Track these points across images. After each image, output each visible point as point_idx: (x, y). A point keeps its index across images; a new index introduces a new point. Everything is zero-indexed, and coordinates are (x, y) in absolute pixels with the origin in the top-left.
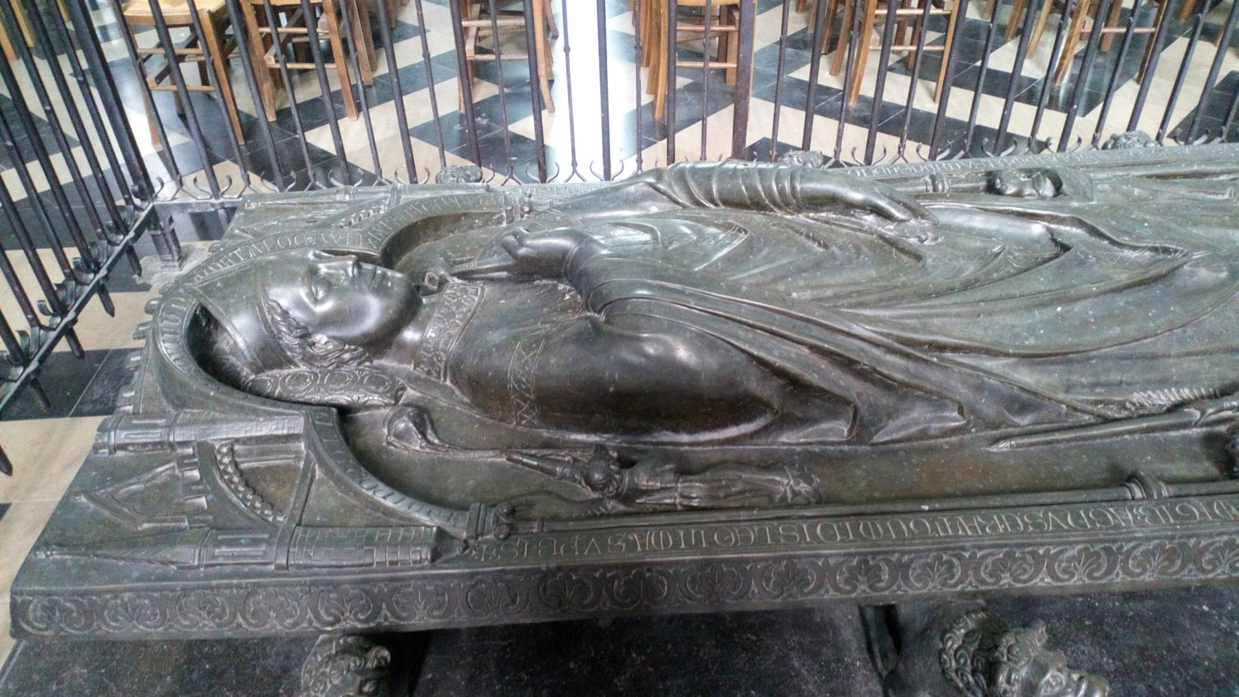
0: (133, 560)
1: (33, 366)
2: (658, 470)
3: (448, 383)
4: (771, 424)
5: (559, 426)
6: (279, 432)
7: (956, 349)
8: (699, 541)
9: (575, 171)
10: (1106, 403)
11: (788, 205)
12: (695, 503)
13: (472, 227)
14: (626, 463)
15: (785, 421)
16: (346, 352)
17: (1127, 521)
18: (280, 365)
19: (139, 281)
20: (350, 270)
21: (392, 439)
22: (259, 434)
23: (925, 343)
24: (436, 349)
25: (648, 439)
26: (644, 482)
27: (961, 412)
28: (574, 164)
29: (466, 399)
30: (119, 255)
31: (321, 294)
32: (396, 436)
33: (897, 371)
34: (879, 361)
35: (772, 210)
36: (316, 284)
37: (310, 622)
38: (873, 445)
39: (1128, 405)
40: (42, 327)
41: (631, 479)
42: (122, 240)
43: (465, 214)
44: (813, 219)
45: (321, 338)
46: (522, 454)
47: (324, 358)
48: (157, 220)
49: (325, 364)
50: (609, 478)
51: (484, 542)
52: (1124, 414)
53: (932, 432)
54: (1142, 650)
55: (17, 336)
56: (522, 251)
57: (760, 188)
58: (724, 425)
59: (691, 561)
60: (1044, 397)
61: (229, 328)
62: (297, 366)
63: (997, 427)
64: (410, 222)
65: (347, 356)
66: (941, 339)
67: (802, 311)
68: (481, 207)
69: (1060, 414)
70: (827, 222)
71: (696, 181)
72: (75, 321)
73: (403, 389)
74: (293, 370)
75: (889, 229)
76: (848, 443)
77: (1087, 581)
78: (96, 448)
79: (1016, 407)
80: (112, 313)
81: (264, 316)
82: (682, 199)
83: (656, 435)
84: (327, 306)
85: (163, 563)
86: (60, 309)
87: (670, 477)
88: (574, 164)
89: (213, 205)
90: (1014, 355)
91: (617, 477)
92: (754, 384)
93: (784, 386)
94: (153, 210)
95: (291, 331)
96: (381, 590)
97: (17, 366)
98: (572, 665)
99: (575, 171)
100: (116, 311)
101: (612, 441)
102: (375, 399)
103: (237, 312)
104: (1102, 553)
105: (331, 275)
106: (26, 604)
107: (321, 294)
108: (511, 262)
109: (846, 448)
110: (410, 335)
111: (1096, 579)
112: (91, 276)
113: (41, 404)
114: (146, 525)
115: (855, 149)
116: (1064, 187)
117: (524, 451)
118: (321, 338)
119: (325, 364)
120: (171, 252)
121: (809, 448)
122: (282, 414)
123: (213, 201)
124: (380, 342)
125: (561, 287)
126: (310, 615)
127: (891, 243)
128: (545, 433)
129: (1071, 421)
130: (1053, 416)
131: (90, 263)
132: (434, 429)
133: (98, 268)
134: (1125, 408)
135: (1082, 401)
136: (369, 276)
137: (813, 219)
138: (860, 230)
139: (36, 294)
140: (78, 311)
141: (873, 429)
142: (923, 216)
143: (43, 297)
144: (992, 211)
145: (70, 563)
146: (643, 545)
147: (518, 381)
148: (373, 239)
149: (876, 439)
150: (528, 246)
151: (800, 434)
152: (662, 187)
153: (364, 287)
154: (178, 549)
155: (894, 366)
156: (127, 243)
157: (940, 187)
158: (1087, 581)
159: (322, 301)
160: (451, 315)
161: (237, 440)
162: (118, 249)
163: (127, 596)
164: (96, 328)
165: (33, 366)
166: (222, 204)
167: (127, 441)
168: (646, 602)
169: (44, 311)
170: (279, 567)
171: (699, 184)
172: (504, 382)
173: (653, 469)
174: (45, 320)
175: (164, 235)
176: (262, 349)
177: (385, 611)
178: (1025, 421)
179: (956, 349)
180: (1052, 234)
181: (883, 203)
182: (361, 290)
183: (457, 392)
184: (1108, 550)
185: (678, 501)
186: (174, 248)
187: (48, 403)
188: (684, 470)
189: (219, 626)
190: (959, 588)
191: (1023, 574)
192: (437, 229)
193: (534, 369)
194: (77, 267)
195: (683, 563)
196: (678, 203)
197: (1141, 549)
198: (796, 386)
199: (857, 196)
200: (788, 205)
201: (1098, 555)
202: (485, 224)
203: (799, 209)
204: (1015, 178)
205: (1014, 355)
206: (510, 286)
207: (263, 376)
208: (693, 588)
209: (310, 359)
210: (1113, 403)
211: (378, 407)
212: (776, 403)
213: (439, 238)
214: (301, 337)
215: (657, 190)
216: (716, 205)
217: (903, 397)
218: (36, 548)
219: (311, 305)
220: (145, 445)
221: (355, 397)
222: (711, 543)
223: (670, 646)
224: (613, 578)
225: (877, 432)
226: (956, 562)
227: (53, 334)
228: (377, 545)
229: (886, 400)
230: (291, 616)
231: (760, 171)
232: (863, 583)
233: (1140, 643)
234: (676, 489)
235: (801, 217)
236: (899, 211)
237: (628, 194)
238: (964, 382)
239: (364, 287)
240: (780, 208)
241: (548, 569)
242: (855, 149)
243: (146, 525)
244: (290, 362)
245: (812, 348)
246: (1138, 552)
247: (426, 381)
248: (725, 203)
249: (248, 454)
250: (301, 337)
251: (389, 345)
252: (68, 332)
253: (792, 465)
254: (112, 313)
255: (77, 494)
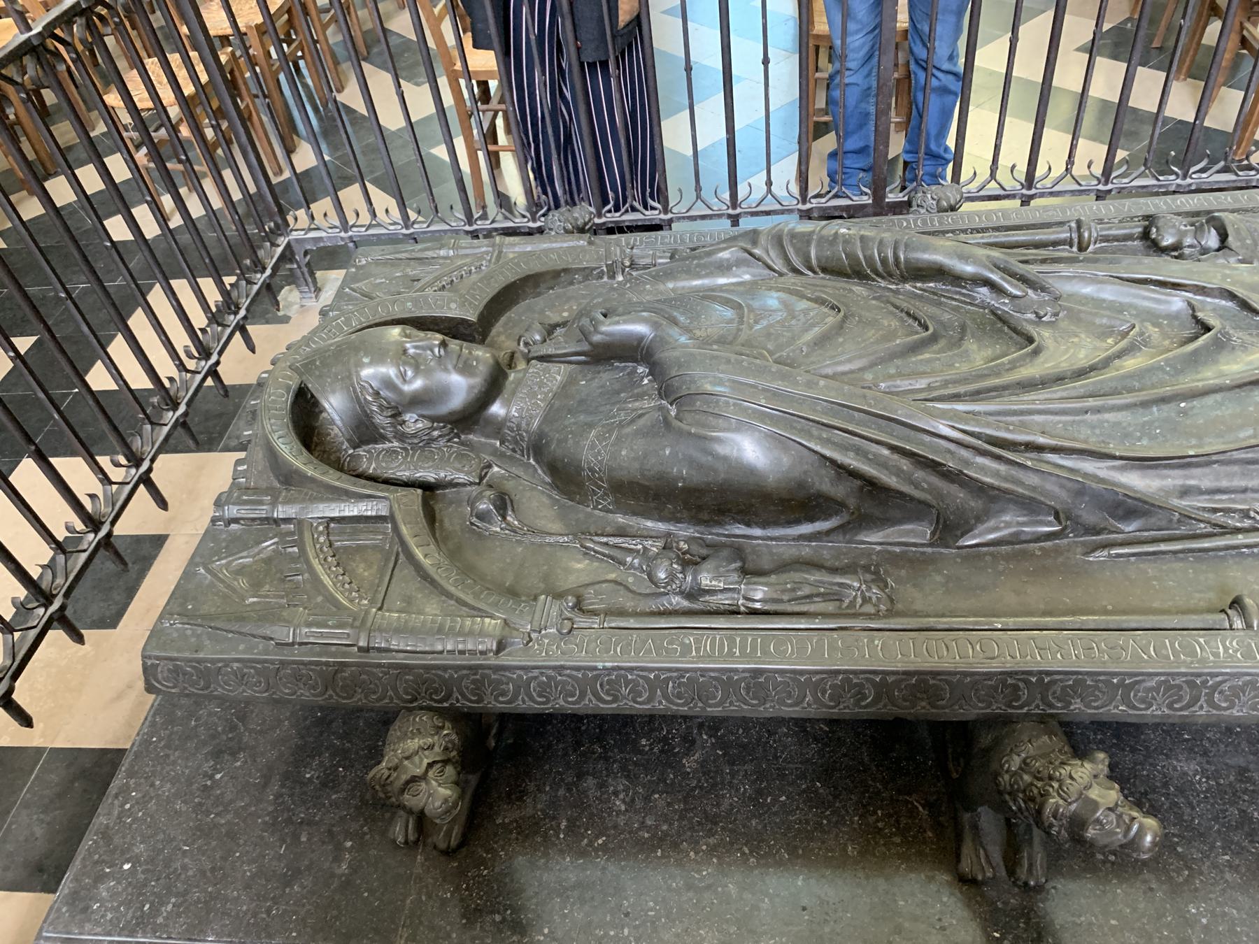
0: (240, 633)
1: (182, 409)
2: (722, 569)
3: (531, 460)
4: (849, 523)
5: (635, 514)
6: (369, 513)
7: (1055, 450)
8: (754, 649)
9: (769, 191)
10: (1227, 511)
11: (891, 275)
12: (758, 606)
13: (572, 283)
14: (689, 562)
15: (862, 521)
16: (435, 429)
17: (1216, 655)
18: (376, 442)
19: (281, 313)
20: (436, 350)
21: (474, 520)
22: (351, 514)
23: (1021, 444)
24: (519, 426)
25: (721, 531)
26: (706, 580)
27: (1057, 517)
28: (698, 188)
29: (548, 479)
30: (258, 293)
31: (410, 373)
32: (477, 517)
33: (986, 475)
34: (967, 463)
35: (874, 280)
36: (405, 363)
37: (391, 699)
38: (959, 548)
39: (1252, 514)
40: (188, 371)
41: (695, 579)
42: (260, 278)
43: (565, 270)
44: (921, 289)
45: (410, 417)
46: (594, 542)
47: (414, 436)
48: (293, 254)
49: (416, 441)
50: (672, 577)
51: (546, 636)
52: (1247, 523)
53: (1023, 537)
54: (1242, 772)
55: (199, 333)
56: (597, 338)
57: (861, 257)
58: (798, 522)
59: (745, 670)
60: (1153, 505)
61: (326, 406)
62: (390, 442)
63: (1098, 533)
64: (508, 282)
65: (436, 433)
66: (1041, 440)
67: (884, 409)
68: (581, 261)
69: (1171, 521)
70: (935, 294)
71: (793, 245)
72: (218, 363)
73: (490, 466)
74: (388, 445)
75: (1004, 305)
76: (931, 545)
77: (1167, 711)
78: (214, 521)
79: (1120, 512)
80: (253, 350)
81: (357, 397)
82: (779, 265)
83: (728, 527)
84: (418, 384)
85: (264, 638)
86: (205, 353)
87: (735, 577)
88: (698, 188)
89: (342, 239)
90: (1121, 458)
91: (680, 576)
92: (825, 483)
93: (861, 488)
94: (289, 245)
95: (382, 411)
96: (451, 676)
97: (168, 410)
98: (644, 742)
99: (769, 191)
100: (257, 350)
101: (684, 532)
102: (462, 477)
103: (334, 392)
104: (1185, 686)
105: (419, 355)
106: (155, 666)
107: (410, 373)
108: (585, 347)
109: (929, 550)
110: (497, 409)
111: (1177, 710)
112: (259, 276)
113: (191, 443)
114: (252, 600)
115: (1014, 166)
116: (1230, 239)
117: (596, 538)
118: (410, 417)
119: (416, 441)
120: (307, 285)
121: (889, 548)
122: (369, 496)
123: (342, 234)
124: (469, 418)
125: (640, 369)
126: (390, 693)
127: (1001, 319)
128: (620, 519)
129: (1183, 530)
130: (1164, 523)
131: (230, 304)
132: (513, 510)
133: (264, 269)
134: (1250, 518)
135: (1198, 509)
136: (455, 357)
137: (921, 289)
138: (971, 304)
139: (181, 340)
140: (220, 353)
141: (959, 533)
142: (1043, 289)
143: (189, 343)
144: (1128, 280)
145: (189, 632)
146: (698, 650)
147: (592, 470)
148: (470, 303)
149: (960, 543)
150: (602, 333)
151: (881, 534)
152: (756, 251)
153: (450, 367)
154: (276, 628)
155: (985, 469)
156: (238, 323)
157: (1086, 235)
158: (1167, 711)
159: (410, 382)
160: (534, 395)
161: (332, 519)
162: (256, 288)
163: (235, 665)
164: (237, 366)
165: (182, 409)
166: (351, 237)
167: (239, 516)
168: (700, 704)
169: (190, 356)
170: (361, 649)
171: (797, 251)
172: (579, 469)
173: (717, 568)
174: (191, 364)
175: (299, 267)
176: (358, 427)
177: (456, 694)
178: (1130, 527)
179: (1055, 450)
180: (1193, 310)
181: (995, 277)
182: (446, 370)
183: (540, 471)
184: (1192, 684)
185: (741, 602)
186: (310, 280)
187: (197, 443)
188: (749, 572)
189: (314, 695)
190: (1025, 710)
191: (1095, 701)
192: (537, 285)
193: (605, 457)
194: (219, 310)
195: (735, 671)
196: (774, 270)
197: (1228, 684)
198: (871, 487)
199: (969, 269)
200: (891, 275)
201: (1180, 687)
202: (586, 278)
203: (904, 279)
204: (1174, 226)
205: (1121, 458)
206: (592, 368)
207: (361, 452)
208: (748, 693)
209: (402, 437)
210: (1235, 511)
211: (464, 485)
212: (852, 502)
213: (539, 294)
214: (393, 416)
215: (751, 254)
216: (814, 272)
217: (993, 499)
218: (161, 617)
219: (401, 385)
220: (253, 519)
221: (442, 475)
222: (765, 652)
223: (741, 731)
224: (667, 680)
225: (962, 535)
226: (1021, 685)
227: (199, 377)
228: (447, 635)
229: (975, 504)
230: (374, 693)
231: (862, 238)
232: (922, 699)
233: (1241, 761)
234: (739, 591)
235: (908, 286)
236: (1015, 287)
237: (722, 260)
238: (1062, 486)
239: (450, 367)
240: (883, 278)
241: (605, 668)
242: (1014, 166)
243: (252, 600)
244: (383, 438)
245: (893, 448)
246: (1225, 687)
247: (511, 458)
248: (824, 270)
249: (342, 533)
250: (393, 416)
251: (476, 422)
252: (213, 372)
253: (866, 569)
254: (253, 350)
255: (197, 565)
